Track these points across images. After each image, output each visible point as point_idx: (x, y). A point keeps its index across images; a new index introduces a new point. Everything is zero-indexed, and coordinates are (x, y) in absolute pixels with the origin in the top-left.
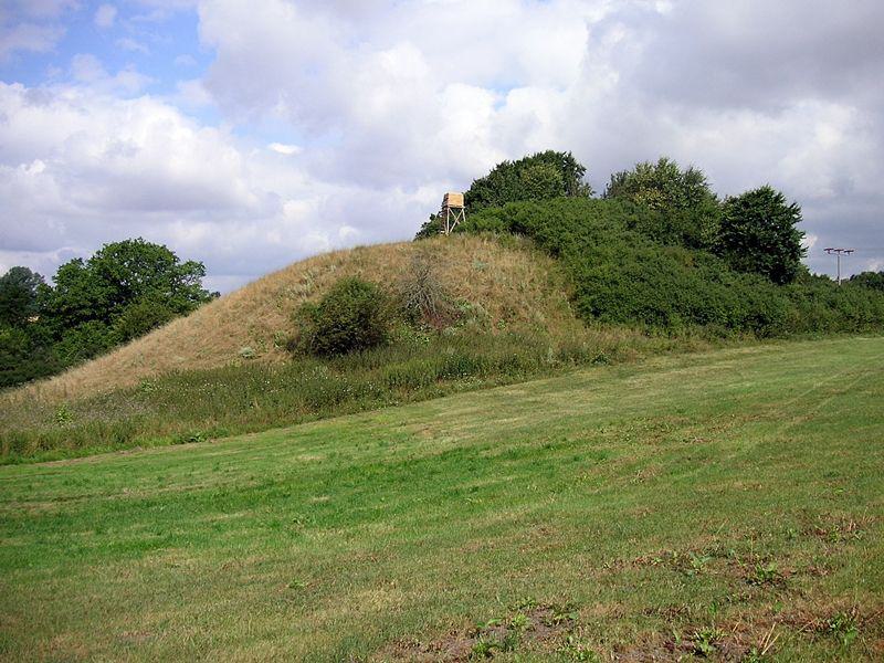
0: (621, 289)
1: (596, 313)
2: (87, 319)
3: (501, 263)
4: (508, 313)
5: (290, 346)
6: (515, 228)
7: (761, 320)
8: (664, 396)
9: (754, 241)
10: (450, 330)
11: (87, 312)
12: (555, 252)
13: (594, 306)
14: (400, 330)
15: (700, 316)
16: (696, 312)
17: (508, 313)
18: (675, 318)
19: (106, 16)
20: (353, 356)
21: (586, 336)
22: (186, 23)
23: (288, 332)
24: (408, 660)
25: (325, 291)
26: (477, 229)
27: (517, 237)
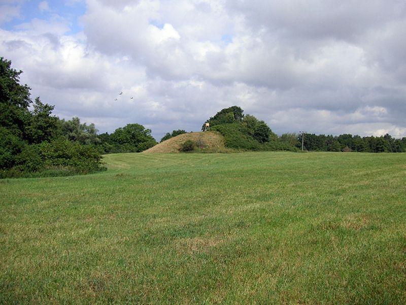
0: (232, 142)
1: (227, 146)
2: (125, 143)
3: (214, 137)
4: (213, 146)
5: (179, 150)
6: (218, 130)
7: (253, 148)
8: (378, 173)
9: (260, 134)
10: (204, 148)
11: (126, 141)
12: (224, 135)
13: (228, 145)
14: (196, 148)
15: (243, 147)
16: (243, 146)
17: (213, 146)
18: (239, 147)
19: (44, 6)
20: (189, 152)
21: (225, 149)
22: (82, 9)
23: (179, 148)
24: (200, 304)
25: (185, 142)
26: (211, 130)
27: (218, 132)
